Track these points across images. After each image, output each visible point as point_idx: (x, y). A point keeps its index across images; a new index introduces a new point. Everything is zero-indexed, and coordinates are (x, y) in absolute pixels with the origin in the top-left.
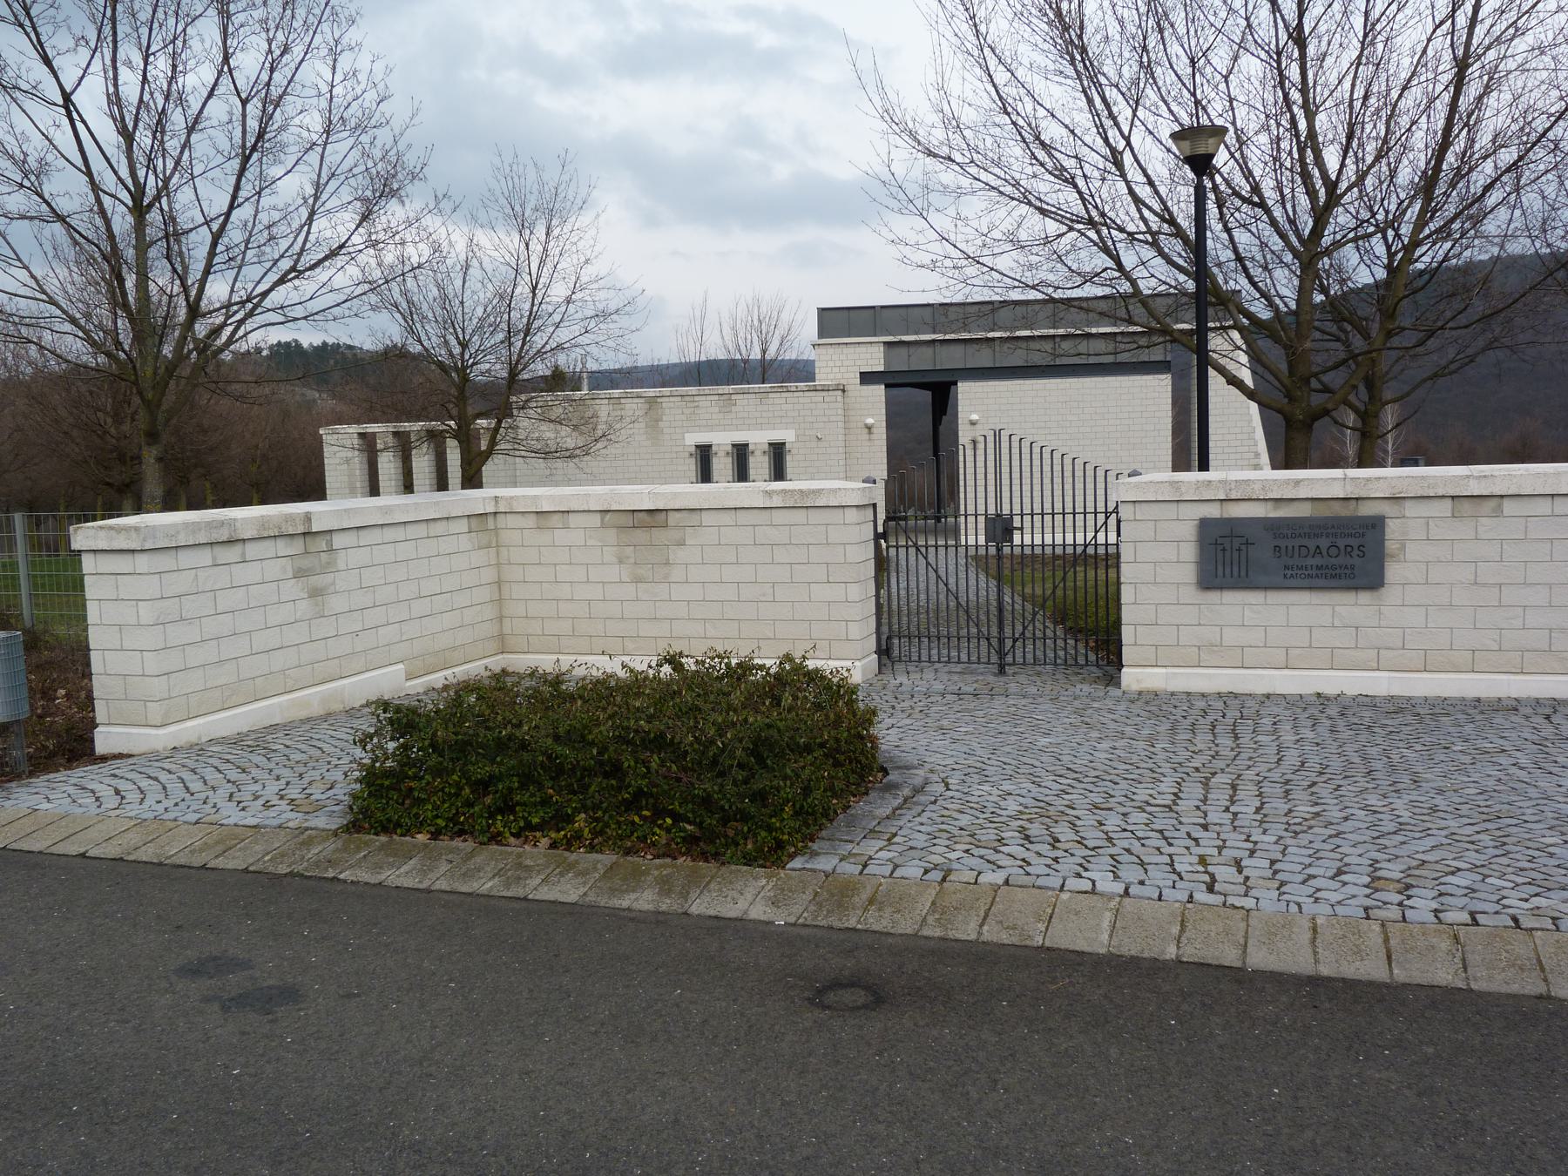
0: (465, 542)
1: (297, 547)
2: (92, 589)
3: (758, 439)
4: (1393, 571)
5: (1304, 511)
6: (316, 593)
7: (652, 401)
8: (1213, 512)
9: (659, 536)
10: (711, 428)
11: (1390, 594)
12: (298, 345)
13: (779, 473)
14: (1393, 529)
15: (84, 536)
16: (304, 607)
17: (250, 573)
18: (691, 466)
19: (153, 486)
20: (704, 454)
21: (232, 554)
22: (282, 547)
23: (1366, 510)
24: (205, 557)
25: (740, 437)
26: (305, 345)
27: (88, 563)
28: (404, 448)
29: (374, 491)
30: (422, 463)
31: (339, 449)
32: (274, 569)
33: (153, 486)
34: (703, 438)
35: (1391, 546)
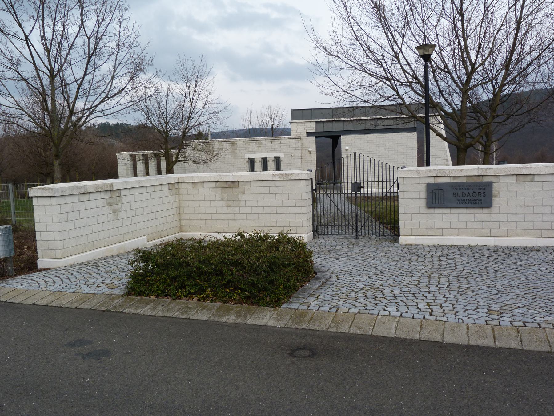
0: (167, 193)
1: (108, 195)
2: (36, 210)
3: (258, 156)
4: (495, 201)
5: (464, 180)
6: (115, 211)
7: (233, 143)
8: (432, 181)
9: (236, 190)
10: (254, 152)
11: (495, 209)
12: (108, 124)
13: (278, 168)
14: (495, 186)
15: (33, 192)
16: (111, 216)
17: (92, 204)
18: (247, 166)
19: (57, 174)
20: (252, 162)
21: (85, 197)
22: (103, 195)
23: (486, 180)
24: (76, 199)
25: (264, 155)
26: (111, 124)
27: (35, 201)
28: (146, 160)
29: (135, 175)
30: (152, 165)
31: (123, 160)
32: (100, 203)
33: (57, 174)
34: (251, 156)
35: (495, 192)
